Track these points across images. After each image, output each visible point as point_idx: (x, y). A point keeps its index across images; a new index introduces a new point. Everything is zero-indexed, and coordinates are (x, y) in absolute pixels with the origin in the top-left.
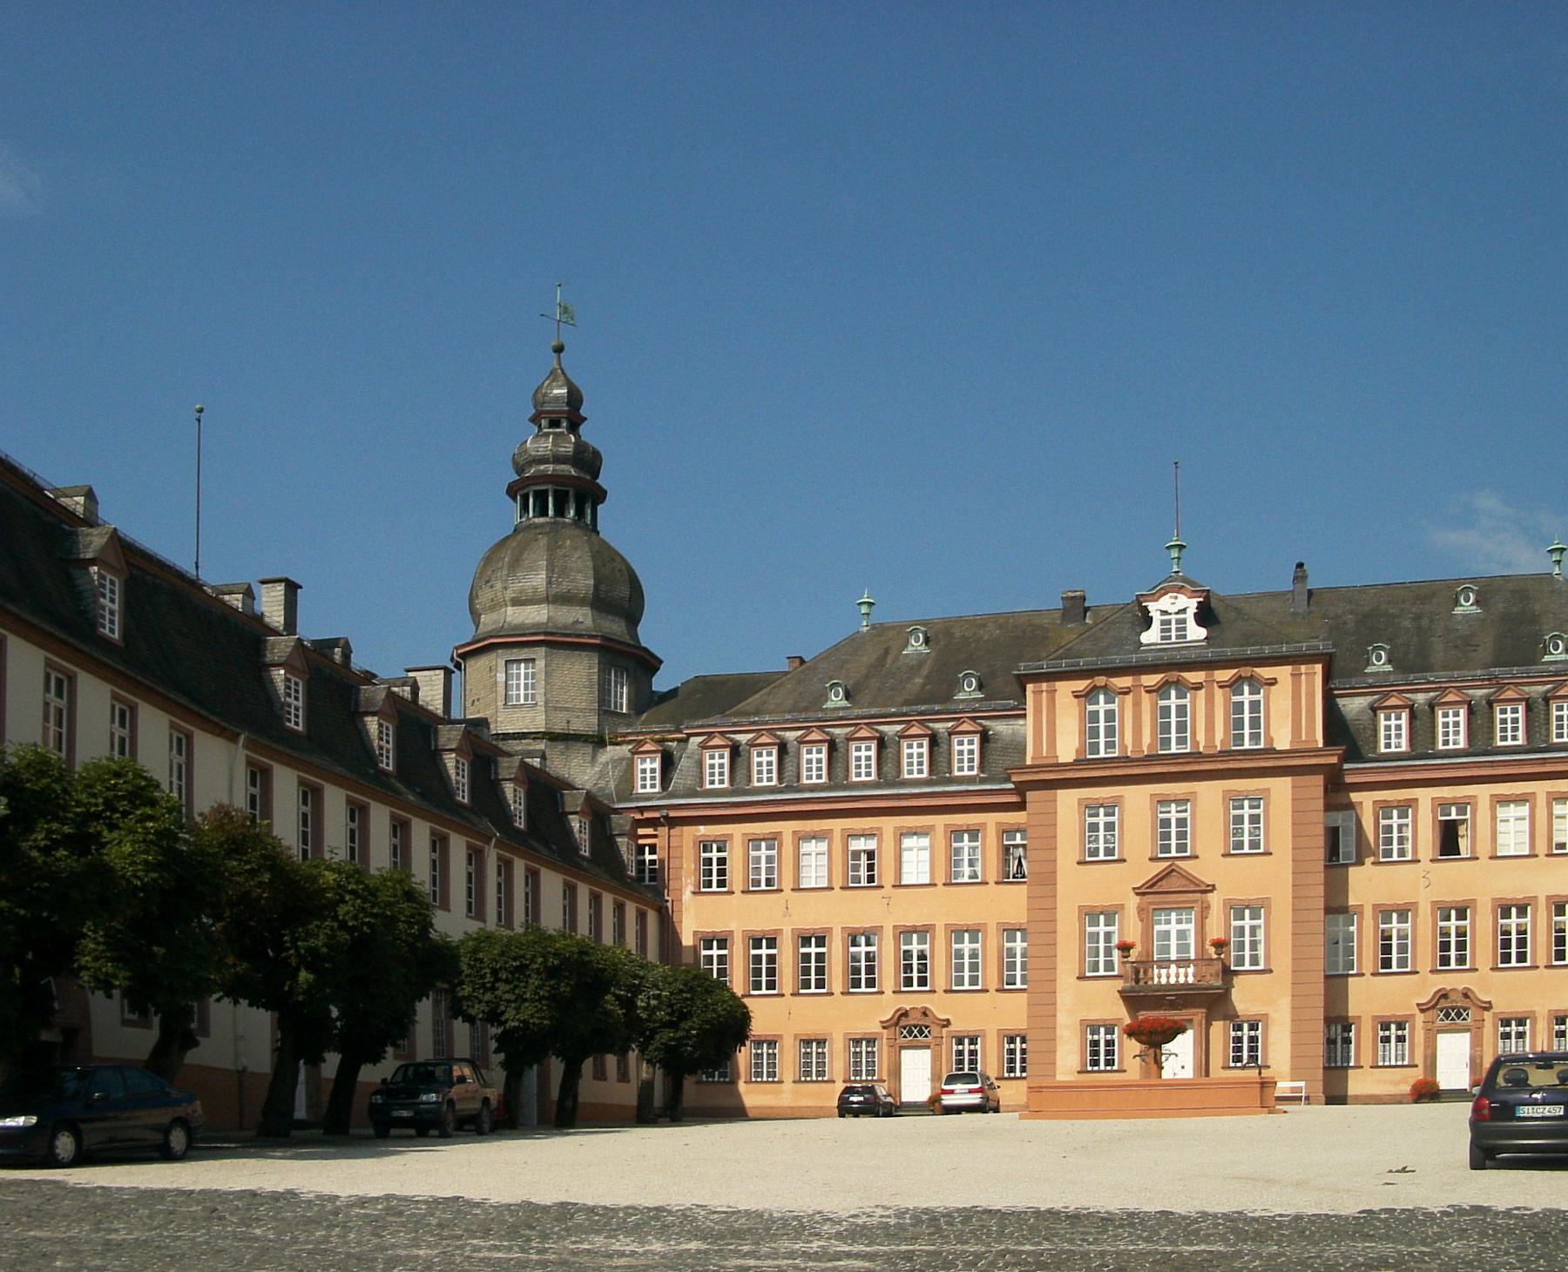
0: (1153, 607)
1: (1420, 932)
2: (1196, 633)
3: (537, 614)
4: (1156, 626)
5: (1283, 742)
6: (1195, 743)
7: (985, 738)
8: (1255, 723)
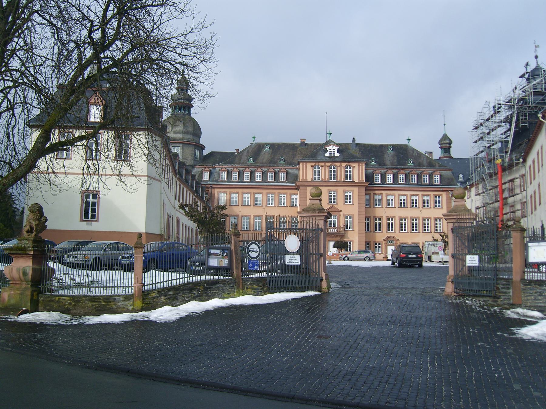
0: (328, 148)
1: (396, 222)
2: (337, 154)
3: (180, 136)
4: (328, 152)
5: (356, 180)
6: (322, 179)
7: (287, 173)
8: (350, 175)
